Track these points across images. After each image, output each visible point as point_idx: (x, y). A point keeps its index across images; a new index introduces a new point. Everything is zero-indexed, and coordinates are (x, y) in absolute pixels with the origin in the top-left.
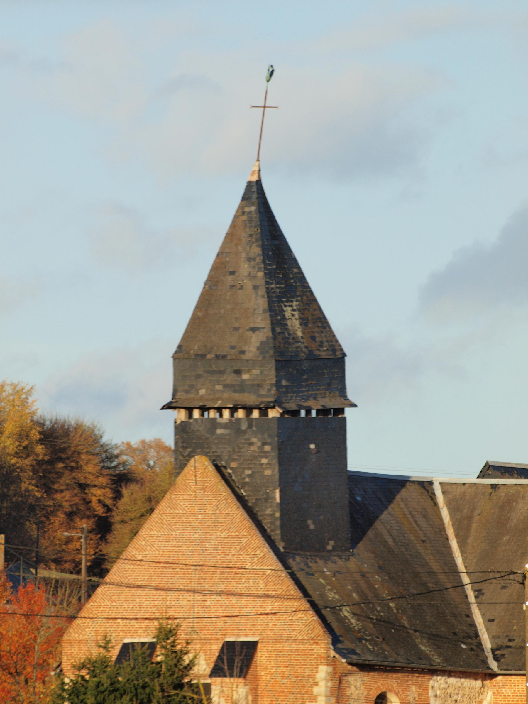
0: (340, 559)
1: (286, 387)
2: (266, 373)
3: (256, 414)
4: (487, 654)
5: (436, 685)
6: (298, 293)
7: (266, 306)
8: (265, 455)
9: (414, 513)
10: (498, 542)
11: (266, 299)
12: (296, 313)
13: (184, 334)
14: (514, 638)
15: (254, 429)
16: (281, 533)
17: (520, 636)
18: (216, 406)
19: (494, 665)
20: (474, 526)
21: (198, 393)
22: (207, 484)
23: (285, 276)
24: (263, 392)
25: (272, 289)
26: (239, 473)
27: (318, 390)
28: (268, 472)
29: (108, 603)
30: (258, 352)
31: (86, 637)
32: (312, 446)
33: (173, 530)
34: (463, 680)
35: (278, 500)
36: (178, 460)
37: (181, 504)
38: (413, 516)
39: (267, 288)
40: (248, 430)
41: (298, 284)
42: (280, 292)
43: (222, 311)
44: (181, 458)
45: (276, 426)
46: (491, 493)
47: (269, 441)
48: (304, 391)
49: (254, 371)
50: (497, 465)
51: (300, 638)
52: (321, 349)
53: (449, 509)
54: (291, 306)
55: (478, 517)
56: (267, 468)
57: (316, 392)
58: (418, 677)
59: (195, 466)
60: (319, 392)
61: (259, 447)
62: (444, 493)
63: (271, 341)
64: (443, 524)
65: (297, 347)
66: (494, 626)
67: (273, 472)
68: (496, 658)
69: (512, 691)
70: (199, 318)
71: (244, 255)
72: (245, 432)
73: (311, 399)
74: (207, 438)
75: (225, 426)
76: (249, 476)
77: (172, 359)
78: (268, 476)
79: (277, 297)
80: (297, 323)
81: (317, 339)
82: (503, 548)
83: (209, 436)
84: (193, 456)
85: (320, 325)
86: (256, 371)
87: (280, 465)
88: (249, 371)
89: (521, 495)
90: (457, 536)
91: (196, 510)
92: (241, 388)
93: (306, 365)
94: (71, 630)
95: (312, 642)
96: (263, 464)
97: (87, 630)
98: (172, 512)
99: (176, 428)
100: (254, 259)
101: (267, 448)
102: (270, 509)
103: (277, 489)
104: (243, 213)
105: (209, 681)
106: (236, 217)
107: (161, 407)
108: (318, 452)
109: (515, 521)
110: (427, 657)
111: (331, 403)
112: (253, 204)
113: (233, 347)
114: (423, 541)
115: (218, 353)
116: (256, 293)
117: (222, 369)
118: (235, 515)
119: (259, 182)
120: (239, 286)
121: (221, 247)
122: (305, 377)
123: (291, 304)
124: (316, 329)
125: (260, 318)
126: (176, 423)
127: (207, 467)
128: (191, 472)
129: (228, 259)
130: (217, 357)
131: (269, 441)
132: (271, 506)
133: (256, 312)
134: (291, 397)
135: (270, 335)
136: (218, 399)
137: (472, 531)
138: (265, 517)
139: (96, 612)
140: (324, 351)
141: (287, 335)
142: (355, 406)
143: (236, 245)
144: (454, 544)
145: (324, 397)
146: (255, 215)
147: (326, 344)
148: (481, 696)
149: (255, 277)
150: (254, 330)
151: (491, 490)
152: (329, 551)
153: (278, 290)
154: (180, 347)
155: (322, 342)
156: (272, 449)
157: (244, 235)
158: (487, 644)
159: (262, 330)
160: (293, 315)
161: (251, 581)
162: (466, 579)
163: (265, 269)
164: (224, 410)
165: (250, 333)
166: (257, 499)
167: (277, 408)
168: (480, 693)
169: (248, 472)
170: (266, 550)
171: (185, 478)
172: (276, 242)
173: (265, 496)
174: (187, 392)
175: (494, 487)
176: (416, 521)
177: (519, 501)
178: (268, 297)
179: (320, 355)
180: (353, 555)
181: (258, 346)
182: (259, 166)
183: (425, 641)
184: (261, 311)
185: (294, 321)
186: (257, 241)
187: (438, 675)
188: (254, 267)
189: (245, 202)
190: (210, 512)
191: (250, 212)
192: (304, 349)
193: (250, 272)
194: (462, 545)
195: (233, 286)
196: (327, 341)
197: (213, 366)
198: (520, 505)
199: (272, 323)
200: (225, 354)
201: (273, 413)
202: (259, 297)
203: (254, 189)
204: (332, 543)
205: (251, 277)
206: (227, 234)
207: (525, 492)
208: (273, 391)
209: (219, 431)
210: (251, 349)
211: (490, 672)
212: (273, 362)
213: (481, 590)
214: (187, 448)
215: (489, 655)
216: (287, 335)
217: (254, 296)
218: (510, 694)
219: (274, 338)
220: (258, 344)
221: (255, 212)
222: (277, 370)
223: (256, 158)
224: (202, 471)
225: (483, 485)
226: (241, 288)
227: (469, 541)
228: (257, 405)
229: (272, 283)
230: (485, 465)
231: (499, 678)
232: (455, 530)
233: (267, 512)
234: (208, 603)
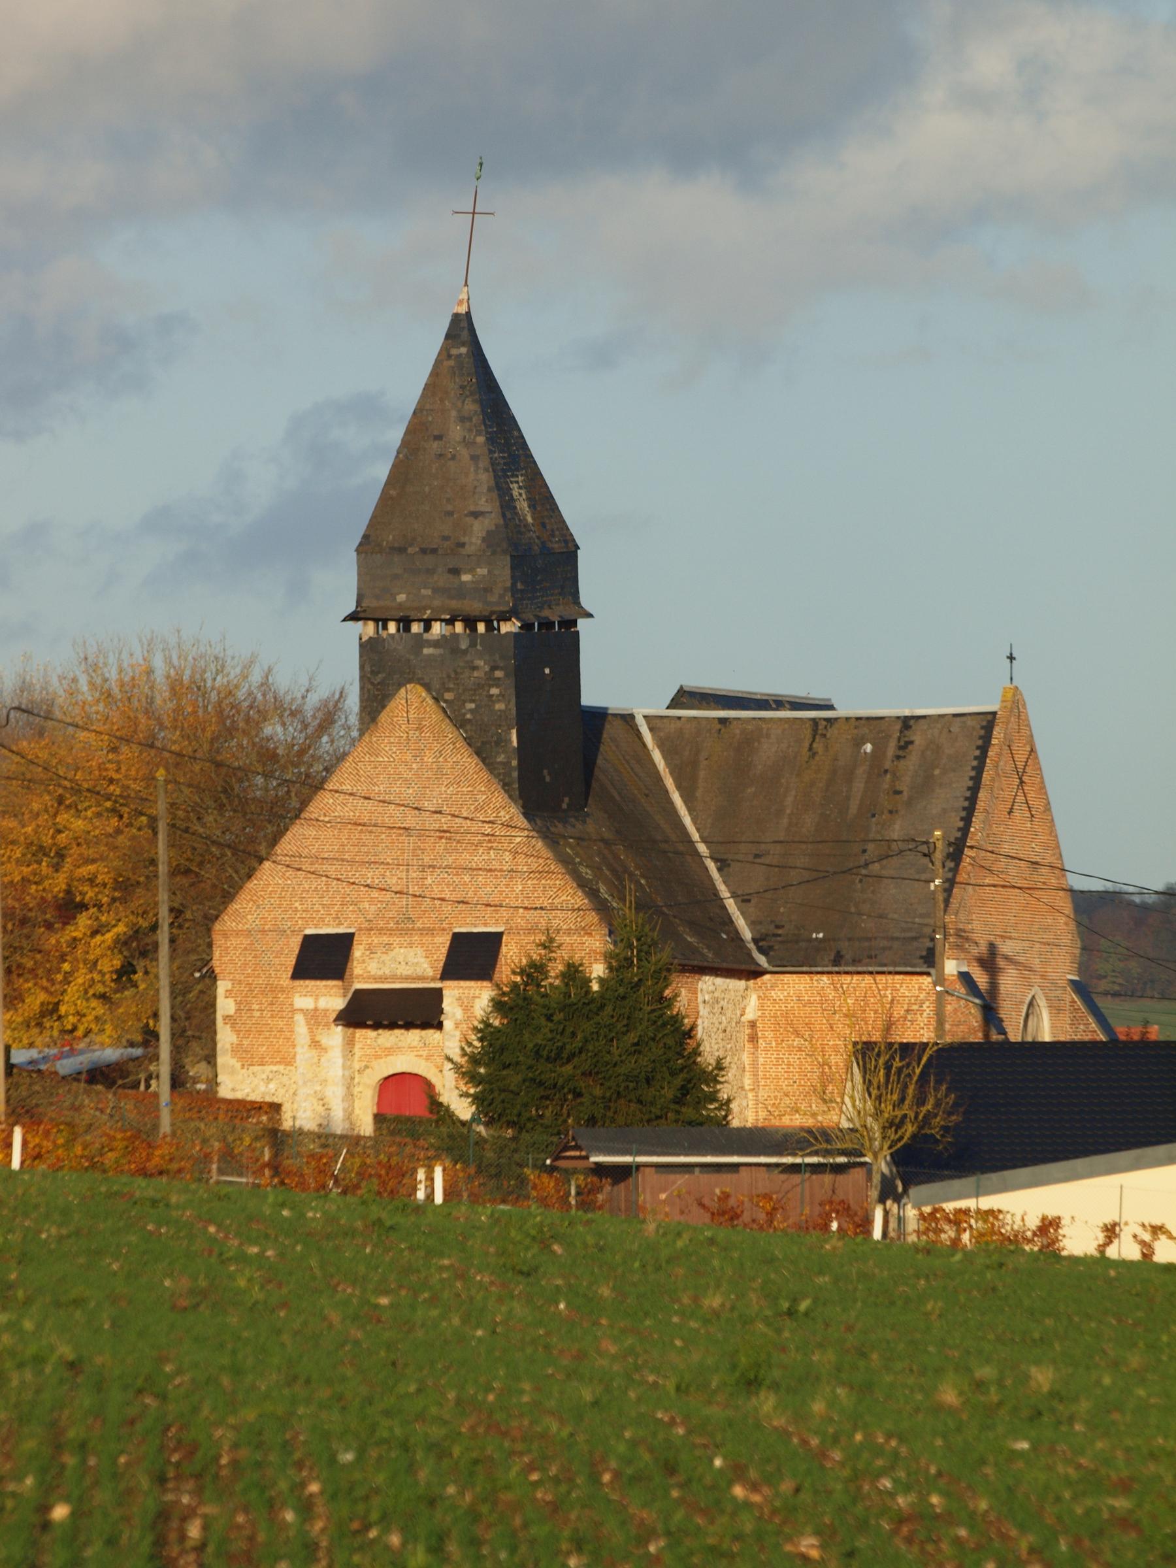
1: (522, 591)
3: (481, 627)
4: (748, 945)
5: (705, 987)
6: (522, 465)
7: (492, 483)
8: (497, 682)
9: (627, 757)
11: (492, 474)
14: (783, 923)
19: (762, 960)
20: (702, 774)
22: (424, 723)
24: (493, 598)
25: (496, 459)
27: (552, 595)
28: (500, 706)
32: (547, 671)
33: (375, 784)
34: (728, 980)
35: (515, 744)
37: (387, 749)
39: (491, 458)
40: (470, 649)
42: (505, 464)
44: (370, 687)
46: (720, 730)
47: (502, 665)
49: (478, 570)
50: (694, 690)
51: (564, 927)
52: (553, 540)
53: (662, 752)
54: (517, 482)
55: (705, 762)
56: (499, 701)
58: (688, 977)
61: (486, 673)
62: (651, 729)
66: (751, 908)
67: (506, 706)
68: (761, 950)
69: (786, 994)
71: (454, 413)
72: (465, 652)
75: (436, 644)
76: (471, 711)
78: (500, 711)
80: (525, 505)
83: (412, 657)
86: (482, 571)
87: (517, 697)
88: (471, 571)
89: (765, 731)
90: (679, 787)
91: (409, 757)
92: (461, 592)
95: (582, 933)
96: (492, 695)
97: (249, 917)
98: (372, 759)
100: (470, 419)
101: (499, 674)
103: (513, 728)
104: (449, 356)
105: (438, 985)
106: (438, 363)
109: (760, 767)
111: (566, 612)
112: (463, 344)
114: (647, 795)
115: (424, 546)
117: (430, 567)
120: (450, 456)
122: (539, 578)
123: (516, 479)
125: (484, 499)
126: (361, 639)
130: (424, 551)
135: (502, 522)
136: (425, 608)
137: (700, 781)
139: (262, 893)
142: (590, 616)
143: (442, 400)
144: (676, 798)
147: (557, 533)
148: (744, 1002)
150: (476, 515)
151: (719, 726)
152: (564, 811)
155: (553, 530)
156: (506, 675)
158: (747, 935)
161: (492, 852)
162: (702, 848)
163: (487, 433)
164: (433, 623)
165: (469, 520)
166: (483, 743)
167: (513, 619)
170: (513, 810)
175: (723, 721)
176: (632, 769)
177: (763, 740)
178: (494, 471)
179: (553, 548)
180: (588, 815)
183: (688, 930)
184: (484, 488)
185: (522, 502)
186: (472, 394)
188: (470, 430)
195: (441, 455)
199: (502, 507)
200: (435, 546)
201: (507, 628)
203: (464, 324)
204: (566, 800)
206: (426, 385)
209: (426, 651)
210: (474, 540)
211: (753, 968)
212: (508, 558)
213: (725, 860)
214: (379, 673)
215: (752, 946)
216: (517, 522)
218: (782, 997)
222: (513, 568)
224: (416, 705)
225: (707, 719)
226: (453, 458)
228: (485, 616)
229: (495, 452)
231: (767, 977)
233: (498, 760)
234: (429, 881)
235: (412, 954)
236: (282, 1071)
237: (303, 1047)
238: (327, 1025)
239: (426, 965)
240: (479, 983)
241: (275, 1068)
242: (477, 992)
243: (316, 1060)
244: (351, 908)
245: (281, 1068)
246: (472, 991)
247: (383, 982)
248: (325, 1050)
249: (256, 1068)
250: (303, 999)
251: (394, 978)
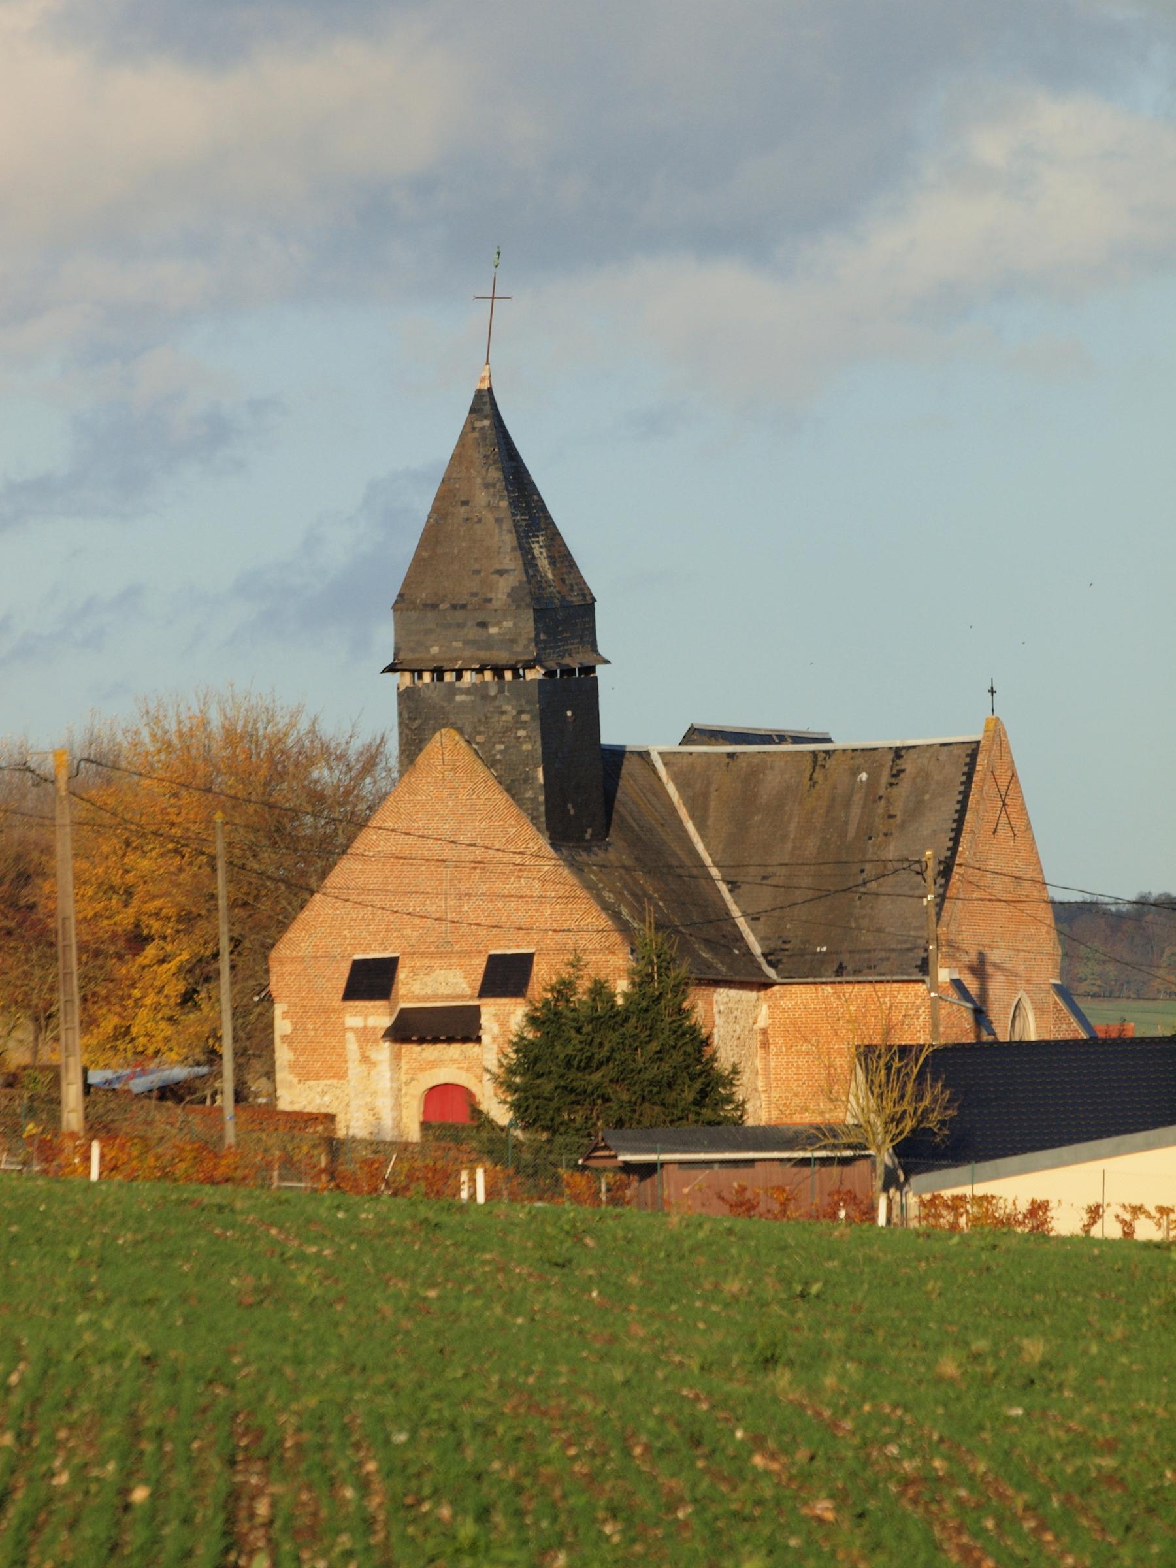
1: (545, 641)
3: (508, 675)
5: (719, 998)
6: (543, 526)
7: (515, 543)
8: (524, 725)
11: (515, 535)
12: (543, 550)
19: (771, 973)
20: (713, 804)
21: (429, 651)
23: (528, 504)
24: (519, 648)
28: (527, 747)
30: (509, 600)
31: (300, 954)
32: (569, 713)
33: (415, 821)
34: (741, 992)
35: (541, 780)
38: (645, 795)
40: (499, 696)
42: (526, 525)
44: (408, 732)
47: (528, 709)
48: (559, 647)
49: (505, 623)
54: (538, 542)
55: (716, 793)
61: (513, 717)
62: (665, 764)
63: (526, 585)
64: (672, 803)
65: (551, 593)
68: (770, 964)
69: (793, 1003)
70: (424, 560)
71: (479, 481)
72: (494, 698)
74: (443, 707)
75: (467, 691)
76: (501, 752)
80: (546, 562)
81: (567, 582)
83: (445, 704)
85: (567, 564)
86: (508, 624)
88: (498, 624)
89: (769, 764)
92: (489, 643)
93: (560, 615)
95: (607, 952)
96: (520, 737)
99: (400, 695)
100: (494, 486)
101: (525, 717)
104: (474, 429)
106: (463, 435)
108: (575, 720)
110: (710, 966)
112: (486, 417)
113: (474, 595)
115: (455, 602)
116: (500, 527)
117: (461, 621)
119: (490, 390)
122: (560, 629)
125: (508, 559)
129: (457, 486)
131: (528, 708)
132: (531, 788)
133: (502, 550)
134: (549, 653)
137: (711, 810)
141: (539, 578)
142: (607, 662)
144: (690, 827)
145: (578, 653)
147: (575, 587)
149: (498, 507)
150: (501, 572)
152: (587, 841)
153: (524, 523)
154: (401, 595)
156: (532, 718)
157: (477, 456)
158: (757, 949)
160: (541, 553)
161: (522, 880)
162: (715, 872)
163: (510, 497)
165: (496, 577)
166: (513, 781)
167: (537, 667)
168: (755, 1007)
169: (502, 747)
172: (514, 464)
174: (413, 650)
175: (731, 755)
177: (767, 772)
178: (517, 532)
186: (495, 462)
187: (721, 987)
189: (474, 415)
191: (483, 428)
192: (557, 595)
194: (701, 827)
195: (468, 519)
196: (577, 584)
199: (525, 564)
200: (464, 602)
202: (505, 532)
203: (487, 399)
204: (589, 831)
207: (772, 761)
209: (459, 698)
210: (500, 596)
211: (763, 980)
212: (531, 611)
213: (736, 882)
214: (415, 719)
215: (762, 960)
217: (497, 531)
220: (508, 590)
222: (536, 621)
225: (716, 754)
226: (480, 521)
229: (517, 515)
231: (776, 988)
234: (466, 908)
238: (376, 1042)
239: (464, 985)
241: (328, 1082)
242: (512, 1008)
243: (366, 1074)
245: (335, 1082)
246: (507, 1008)
249: (312, 1083)
251: (436, 997)
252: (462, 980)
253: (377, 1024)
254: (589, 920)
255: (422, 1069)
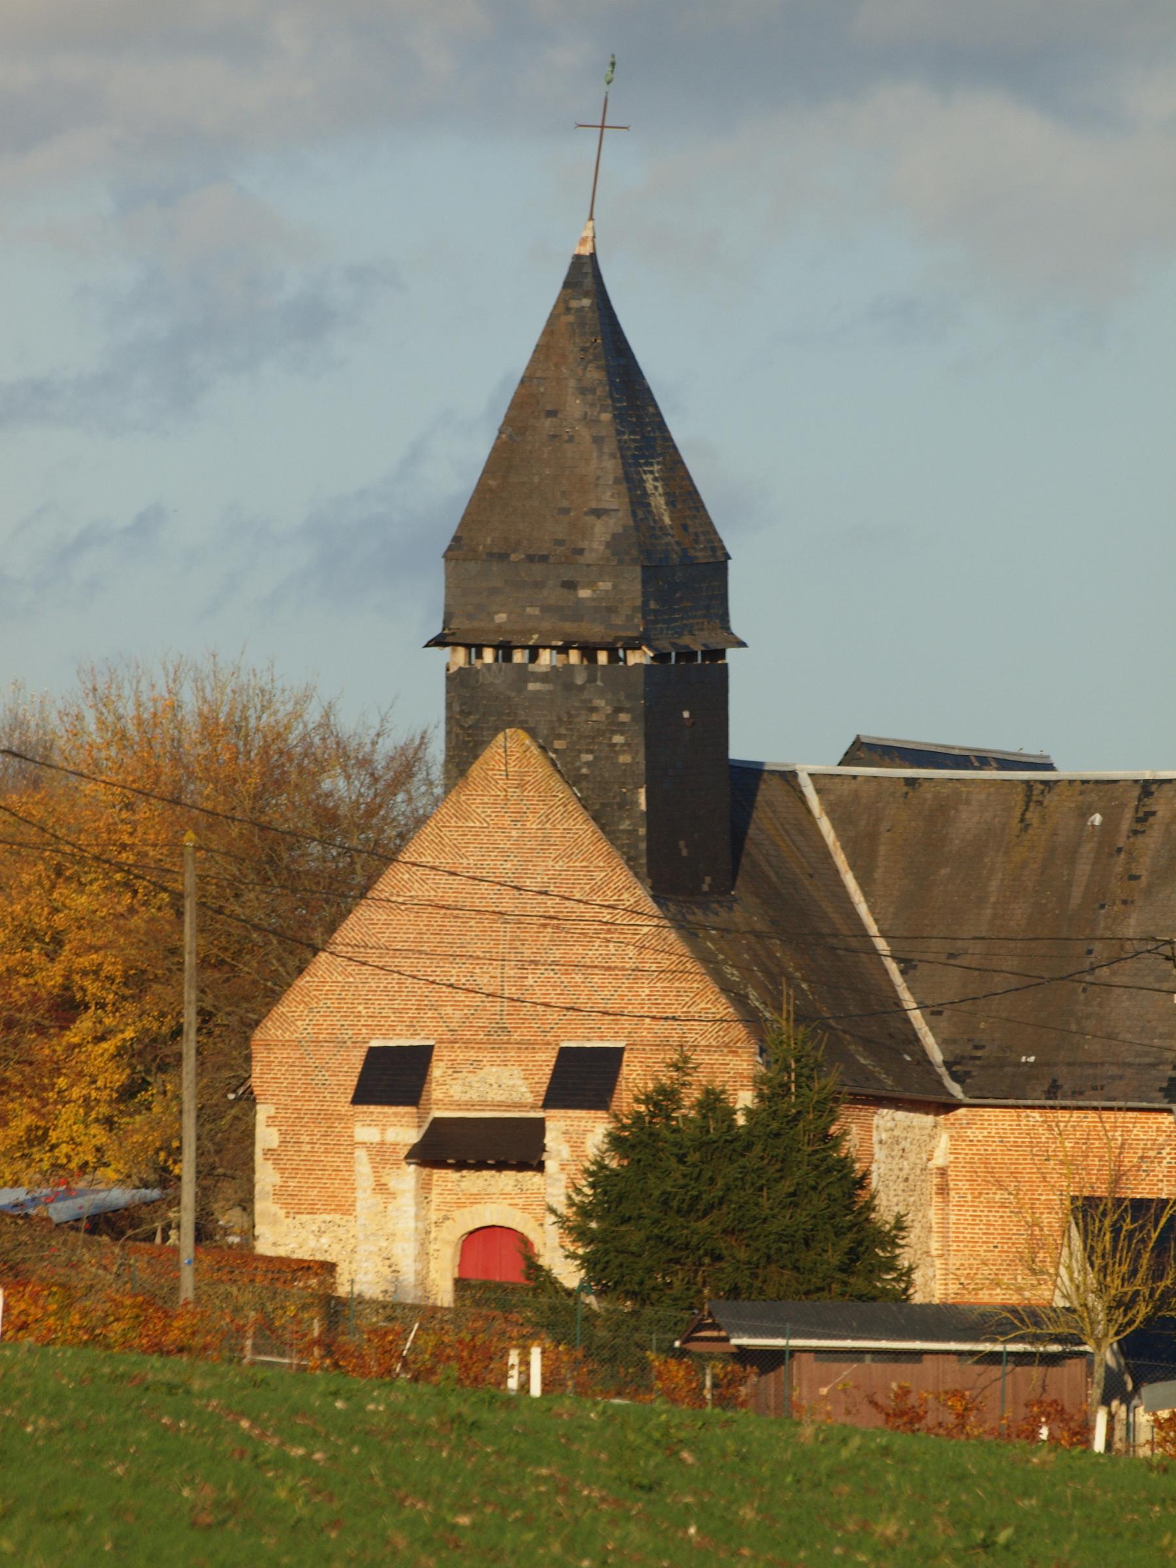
0: (721, 907)
1: (655, 611)
2: (623, 587)
3: (602, 657)
4: (938, 1070)
6: (659, 450)
7: (620, 473)
8: (621, 728)
9: (787, 827)
10: (931, 878)
13: (463, 518)
14: (983, 1043)
15: (599, 683)
16: (649, 862)
17: (993, 1040)
18: (531, 643)
19: (956, 1089)
20: (882, 850)
21: (493, 620)
24: (618, 621)
25: (625, 442)
26: (569, 759)
28: (624, 759)
29: (340, 979)
32: (686, 714)
34: (912, 1115)
35: (643, 807)
36: (453, 736)
37: (479, 811)
38: (786, 831)
39: (619, 441)
40: (588, 685)
41: (658, 434)
42: (637, 448)
43: (536, 479)
45: (642, 680)
49: (601, 584)
51: (703, 1043)
54: (652, 472)
56: (624, 752)
57: (691, 621)
58: (860, 1110)
59: (505, 747)
60: (695, 621)
61: (608, 716)
62: (818, 791)
64: (825, 846)
66: (943, 1022)
68: (955, 1077)
71: (572, 383)
72: (581, 688)
73: (686, 633)
75: (544, 677)
76: (588, 764)
77: (443, 560)
78: (625, 764)
79: (633, 456)
80: (661, 501)
82: (942, 888)
83: (513, 694)
84: (503, 729)
87: (647, 747)
88: (591, 585)
90: (853, 866)
91: (507, 822)
92: (577, 612)
94: (269, 1024)
95: (726, 1050)
97: (299, 1023)
99: (450, 678)
101: (624, 717)
102: (628, 822)
104: (568, 310)
105: (540, 1114)
106: (553, 318)
107: (425, 643)
111: (715, 643)
113: (559, 542)
114: (811, 876)
115: (531, 552)
118: (581, 832)
120: (566, 437)
121: (528, 368)
122: (678, 595)
124: (688, 513)
125: (609, 494)
126: (448, 670)
127: (528, 748)
128: (498, 757)
129: (542, 389)
130: (530, 559)
134: (662, 629)
138: (618, 835)
139: (317, 993)
140: (702, 550)
141: (652, 524)
142: (742, 644)
143: (557, 365)
145: (702, 630)
146: (590, 315)
147: (702, 538)
149: (597, 421)
150: (598, 513)
151: (906, 789)
152: (706, 893)
153: (633, 445)
154: (457, 539)
156: (633, 719)
159: (613, 513)
162: (881, 945)
163: (615, 408)
164: (541, 650)
165: (590, 519)
166: (603, 805)
167: (644, 648)
168: (932, 1137)
171: (485, 767)
173: (618, 800)
174: (470, 617)
175: (911, 782)
176: (793, 841)
178: (623, 457)
179: (697, 558)
180: (735, 900)
181: (608, 543)
182: (593, 228)
188: (592, 405)
189: (569, 291)
190: (534, 826)
192: (676, 547)
193: (586, 414)
195: (555, 436)
197: (523, 575)
198: (964, 816)
199: (632, 503)
200: (545, 553)
201: (636, 658)
202: (606, 457)
203: (588, 269)
205: (589, 421)
206: (537, 346)
208: (638, 619)
209: (531, 686)
210: (595, 545)
211: (944, 1099)
212: (639, 569)
214: (470, 713)
215: (942, 1071)
217: (595, 455)
219: (637, 528)
220: (608, 538)
221: (590, 308)
222: (645, 583)
223: (588, 215)
225: (890, 779)
226: (571, 439)
227: (876, 876)
229: (623, 433)
230: (854, 743)
231: (962, 1111)
232: (848, 857)
233: (622, 827)
234: (530, 981)
235: (507, 1074)
236: (339, 1222)
237: (365, 1191)
238: (396, 1163)
239: (524, 1089)
240: (592, 1113)
241: (328, 1218)
242: (590, 1124)
243: (381, 1208)
244: (429, 1015)
245: (336, 1217)
246: (583, 1123)
247: (468, 1110)
248: (393, 1195)
249: (305, 1218)
250: (366, 1129)
251: (483, 1105)
252: (520, 1082)
253: (399, 1139)
254: (703, 1005)
255: (460, 1205)
